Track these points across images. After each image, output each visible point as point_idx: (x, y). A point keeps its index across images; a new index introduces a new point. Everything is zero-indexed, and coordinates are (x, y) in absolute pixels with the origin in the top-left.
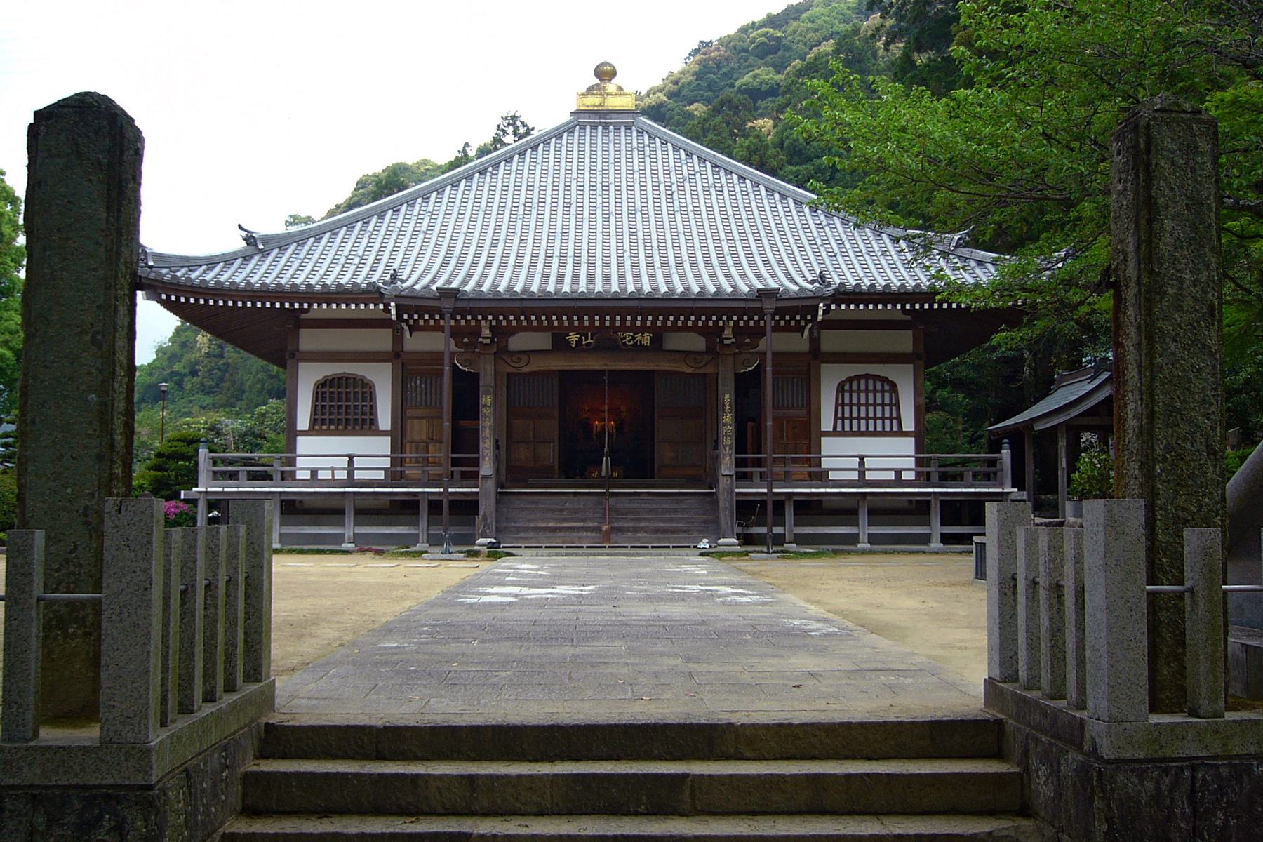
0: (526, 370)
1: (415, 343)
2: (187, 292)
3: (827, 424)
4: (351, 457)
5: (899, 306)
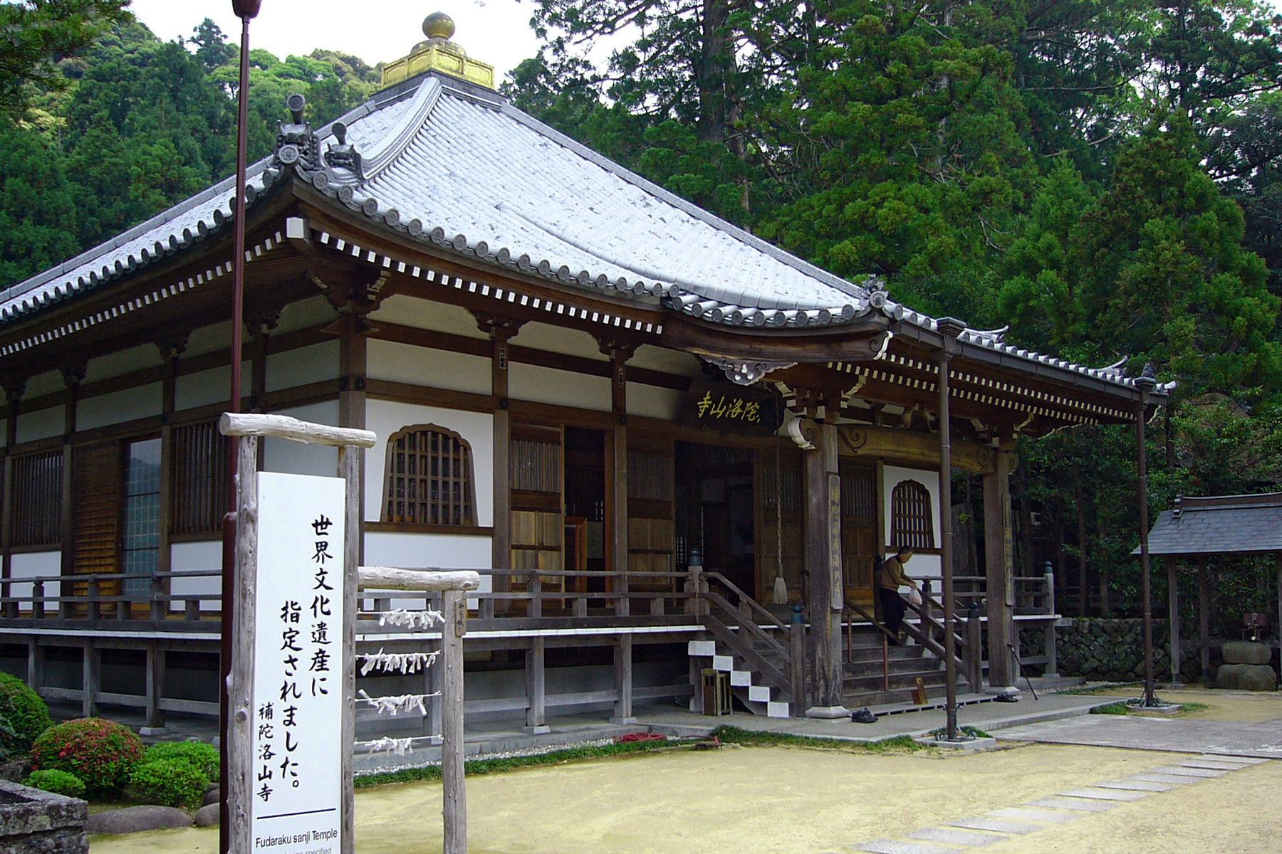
0: (861, 452)
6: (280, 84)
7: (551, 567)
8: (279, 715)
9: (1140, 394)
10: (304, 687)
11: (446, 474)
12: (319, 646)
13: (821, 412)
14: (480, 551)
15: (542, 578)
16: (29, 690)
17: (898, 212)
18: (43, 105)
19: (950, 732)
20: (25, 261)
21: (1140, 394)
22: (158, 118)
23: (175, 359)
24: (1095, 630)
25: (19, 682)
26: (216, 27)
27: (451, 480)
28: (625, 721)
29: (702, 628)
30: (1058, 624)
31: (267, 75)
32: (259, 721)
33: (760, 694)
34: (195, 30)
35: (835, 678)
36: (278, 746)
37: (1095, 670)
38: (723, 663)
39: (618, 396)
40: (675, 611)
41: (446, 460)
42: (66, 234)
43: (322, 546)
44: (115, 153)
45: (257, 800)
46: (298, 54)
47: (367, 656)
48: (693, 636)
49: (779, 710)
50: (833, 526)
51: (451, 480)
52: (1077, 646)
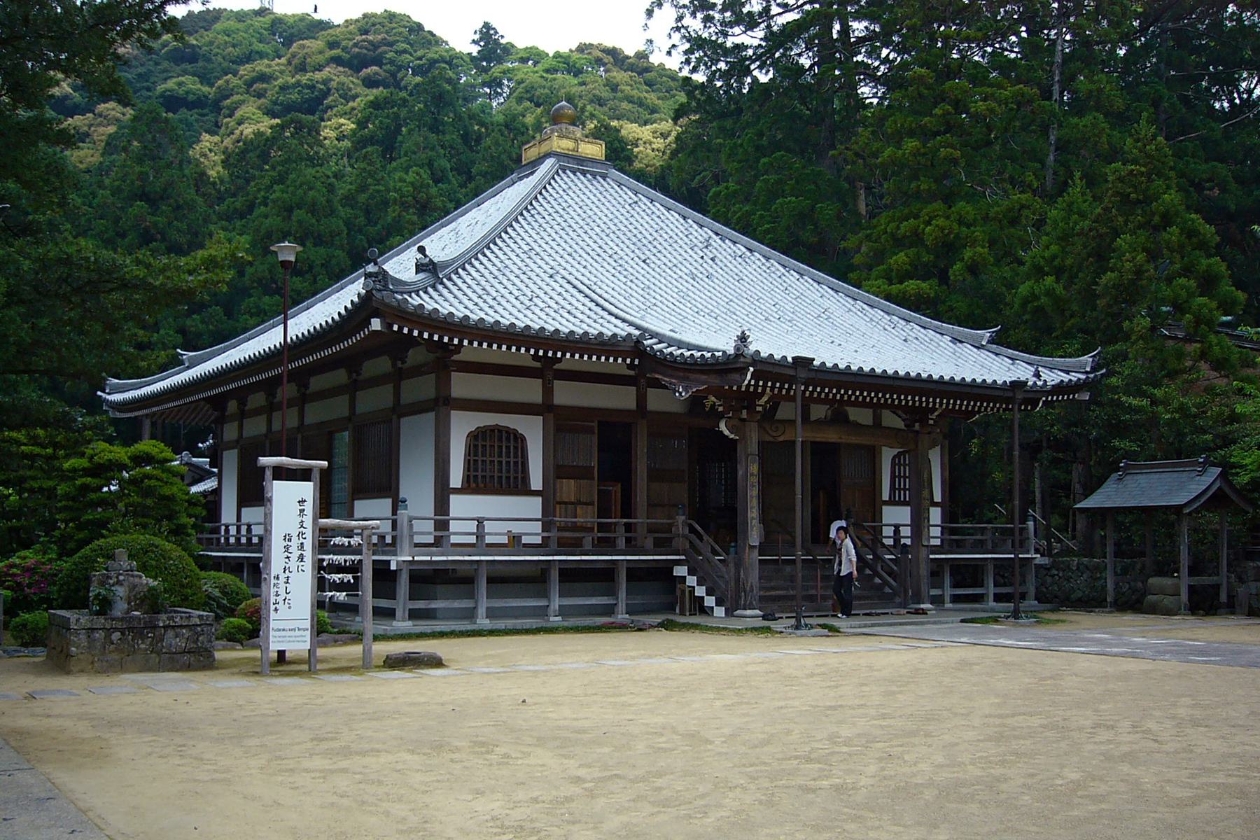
0: (781, 439)
1: (567, 394)
2: (442, 328)
3: (886, 497)
4: (480, 522)
5: (532, 351)
6: (546, 79)
7: (587, 517)
8: (282, 579)
9: (1013, 391)
10: (293, 568)
11: (508, 456)
12: (300, 552)
13: (744, 414)
14: (532, 506)
15: (558, 524)
16: (244, 586)
17: (942, 229)
18: (346, 113)
19: (797, 627)
20: (307, 276)
21: (1013, 391)
22: (417, 144)
23: (356, 380)
24: (1081, 567)
25: (237, 580)
26: (494, 29)
27: (512, 460)
28: (620, 616)
29: (683, 557)
30: (1037, 562)
31: (537, 72)
32: (273, 581)
33: (710, 601)
34: (475, 32)
35: (752, 590)
36: (282, 591)
37: (1080, 600)
38: (692, 581)
39: (641, 399)
40: (662, 545)
41: (508, 448)
42: (338, 252)
43: (302, 511)
44: (378, 182)
45: (272, 612)
46: (564, 49)
47: (324, 557)
48: (678, 563)
49: (720, 612)
50: (752, 490)
51: (512, 460)
52: (1068, 580)
